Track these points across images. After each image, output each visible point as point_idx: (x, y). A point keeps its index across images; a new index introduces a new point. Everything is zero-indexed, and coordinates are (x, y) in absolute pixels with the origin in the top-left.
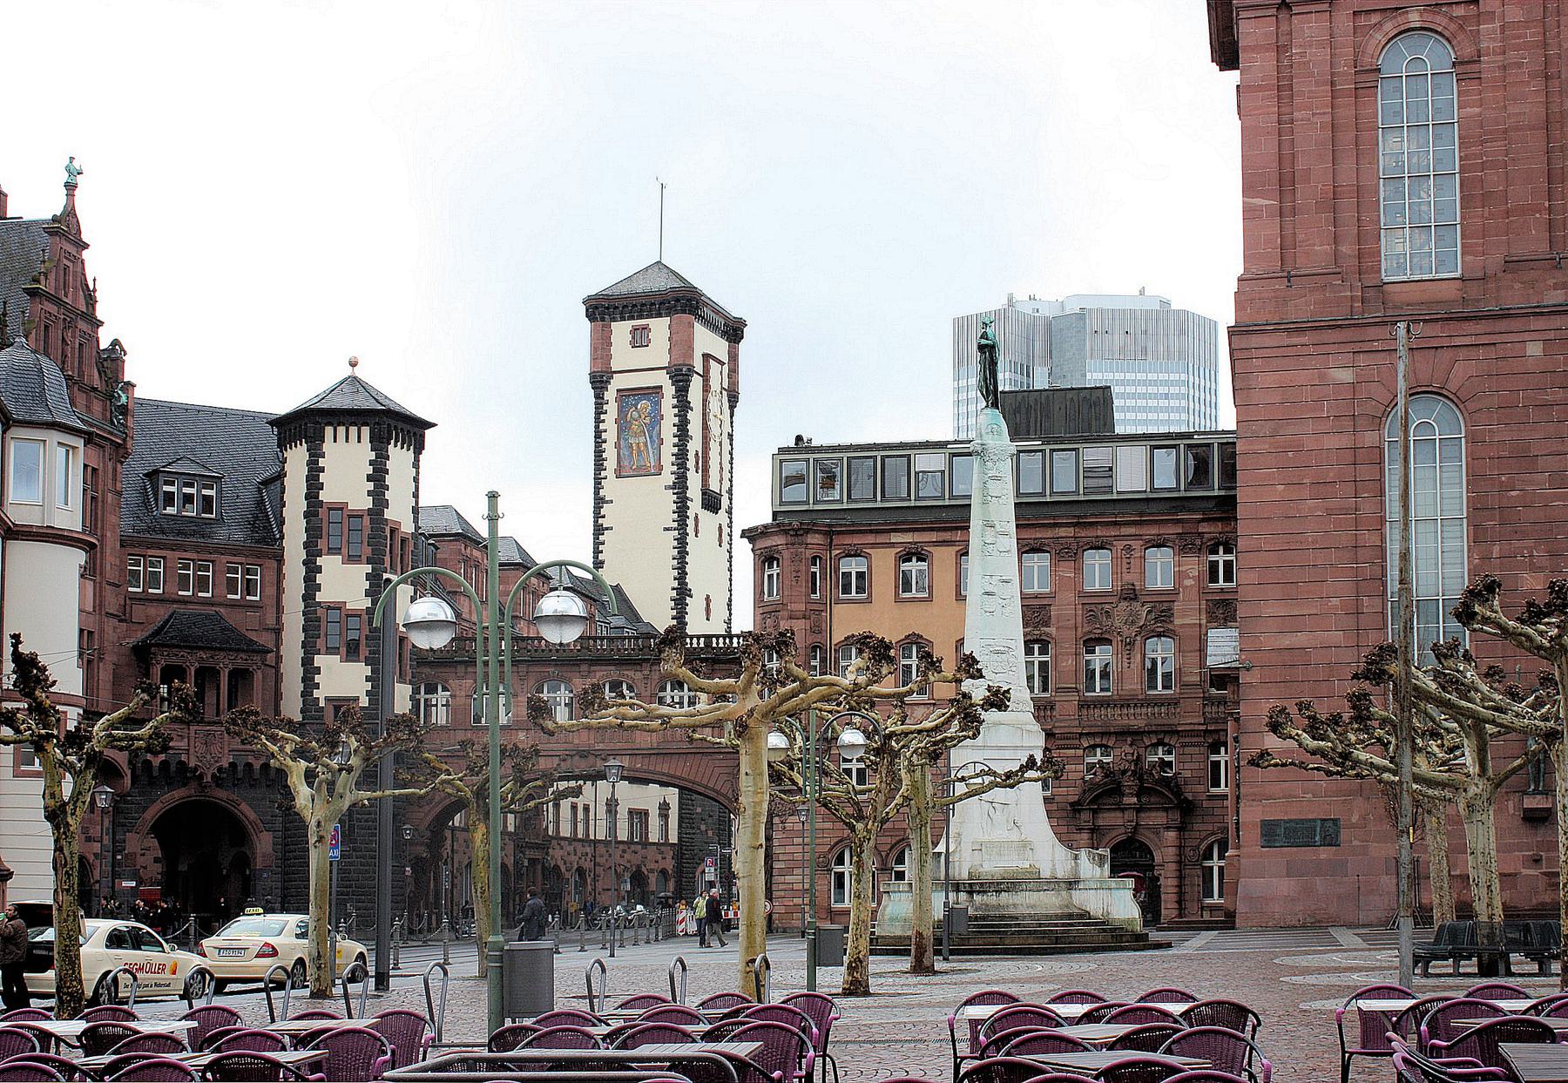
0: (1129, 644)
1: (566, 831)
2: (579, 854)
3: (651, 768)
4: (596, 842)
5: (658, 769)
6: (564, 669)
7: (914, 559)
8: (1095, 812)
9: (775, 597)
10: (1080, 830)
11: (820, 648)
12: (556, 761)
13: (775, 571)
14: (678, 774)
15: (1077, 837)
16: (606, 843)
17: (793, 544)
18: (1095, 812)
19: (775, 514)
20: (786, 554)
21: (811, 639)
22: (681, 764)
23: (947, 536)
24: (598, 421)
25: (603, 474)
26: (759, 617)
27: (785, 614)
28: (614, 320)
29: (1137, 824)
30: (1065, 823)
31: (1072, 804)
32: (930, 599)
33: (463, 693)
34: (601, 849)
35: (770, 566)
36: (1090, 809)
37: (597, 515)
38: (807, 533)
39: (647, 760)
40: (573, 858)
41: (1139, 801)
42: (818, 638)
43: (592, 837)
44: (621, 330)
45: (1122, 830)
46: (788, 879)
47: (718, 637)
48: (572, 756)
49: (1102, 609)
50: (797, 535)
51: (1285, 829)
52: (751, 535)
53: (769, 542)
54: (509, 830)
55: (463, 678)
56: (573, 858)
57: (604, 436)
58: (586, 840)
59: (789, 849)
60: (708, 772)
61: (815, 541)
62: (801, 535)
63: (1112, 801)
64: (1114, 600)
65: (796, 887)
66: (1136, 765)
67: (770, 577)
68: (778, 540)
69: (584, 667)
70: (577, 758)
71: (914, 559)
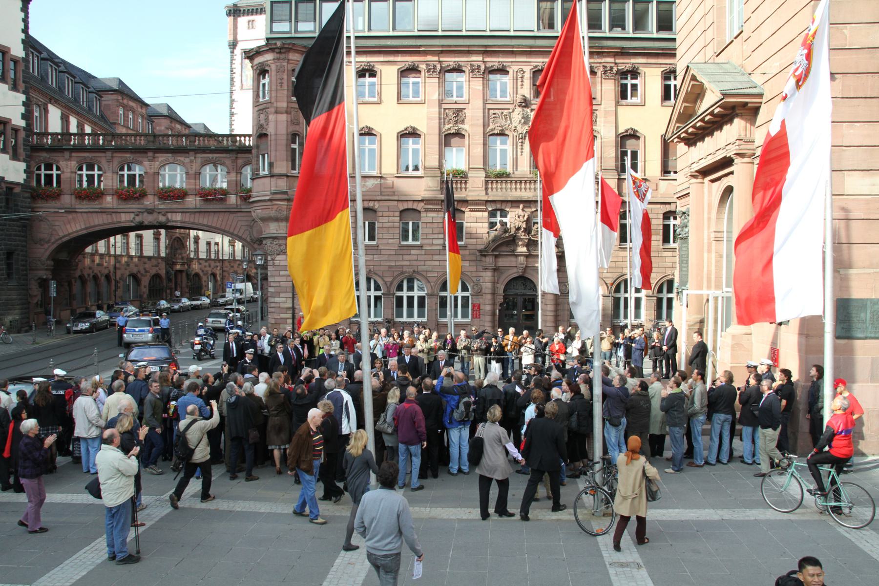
0: (522, 138)
1: (203, 255)
2: (212, 266)
3: (196, 221)
4: (223, 260)
5: (201, 222)
6: (138, 155)
7: (367, 75)
8: (496, 256)
9: (267, 98)
10: (486, 269)
11: (299, 135)
12: (132, 215)
13: (267, 81)
14: (214, 225)
15: (483, 274)
16: (229, 261)
17: (278, 59)
18: (496, 256)
19: (268, 39)
20: (273, 67)
21: (293, 129)
22: (216, 219)
23: (391, 58)
24: (232, 63)
25: (234, 88)
26: (256, 114)
27: (272, 110)
28: (239, 16)
29: (526, 267)
30: (474, 264)
31: (480, 251)
32: (379, 103)
33: (69, 170)
34: (227, 264)
35: (264, 78)
36: (493, 255)
37: (231, 108)
38: (289, 52)
39: (193, 216)
40: (208, 269)
41: (528, 250)
42: (297, 128)
43: (221, 258)
44: (243, 21)
45: (515, 270)
46: (277, 300)
47: (245, 136)
48: (142, 212)
49: (502, 113)
50: (280, 53)
51: (872, 312)
52: (250, 55)
53: (259, 60)
54: (241, 244)
55: (69, 160)
56: (208, 269)
57: (234, 71)
58: (217, 260)
59: (277, 279)
60: (234, 224)
61: (295, 58)
62: (284, 53)
63: (508, 249)
64: (511, 107)
65: (282, 305)
66: (527, 224)
67: (264, 85)
68: (268, 57)
69: (150, 154)
70: (145, 214)
71: (367, 75)
